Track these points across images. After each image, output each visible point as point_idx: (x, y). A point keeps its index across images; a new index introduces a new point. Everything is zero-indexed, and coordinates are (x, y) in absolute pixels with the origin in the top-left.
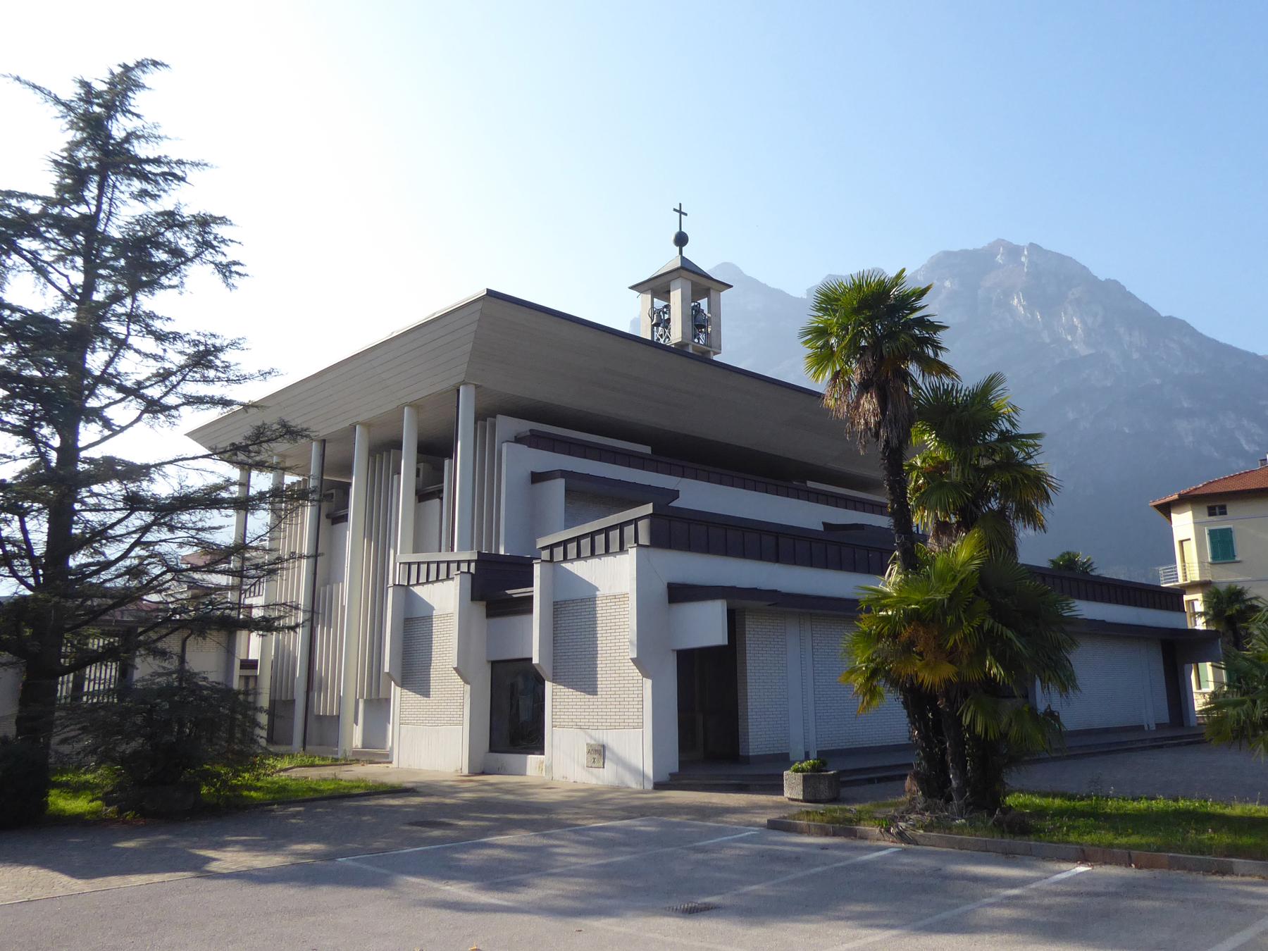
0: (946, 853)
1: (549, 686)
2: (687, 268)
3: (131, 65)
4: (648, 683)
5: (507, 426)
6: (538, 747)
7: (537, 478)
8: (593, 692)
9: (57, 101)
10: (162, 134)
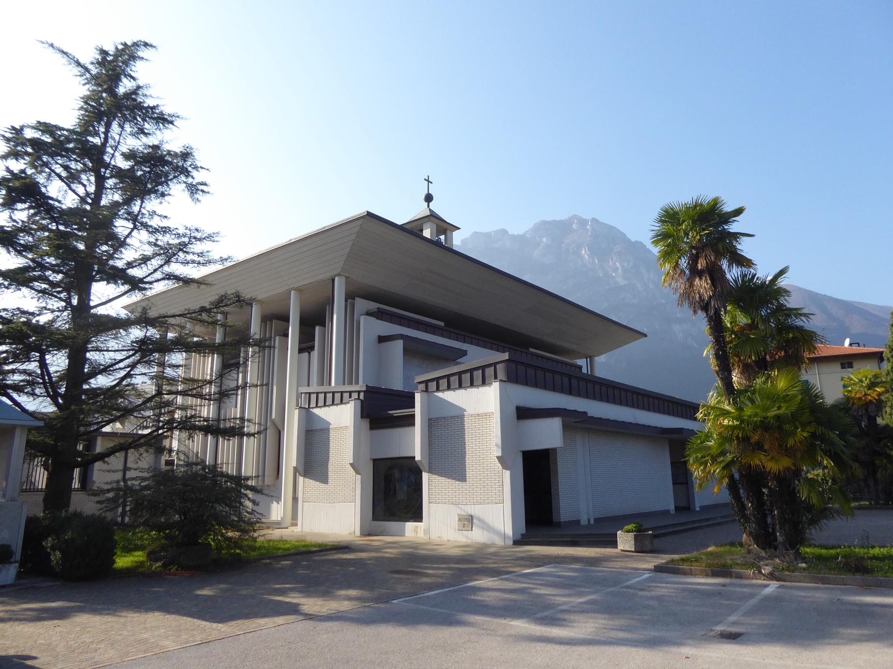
0: (826, 588)
1: (425, 476)
2: (433, 216)
3: (129, 43)
4: (507, 473)
5: (362, 304)
6: (417, 515)
7: (382, 339)
8: (462, 478)
9: (78, 64)
10: (148, 94)
